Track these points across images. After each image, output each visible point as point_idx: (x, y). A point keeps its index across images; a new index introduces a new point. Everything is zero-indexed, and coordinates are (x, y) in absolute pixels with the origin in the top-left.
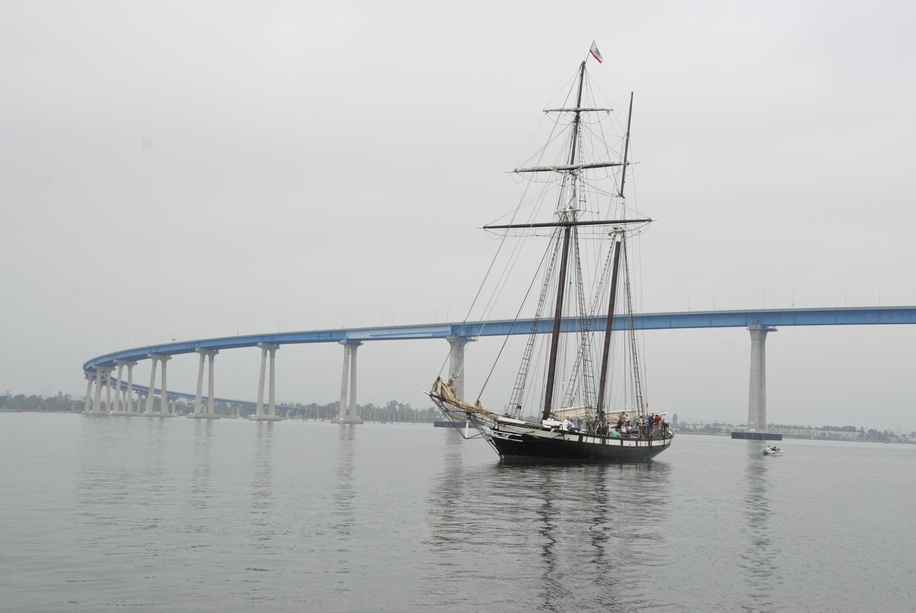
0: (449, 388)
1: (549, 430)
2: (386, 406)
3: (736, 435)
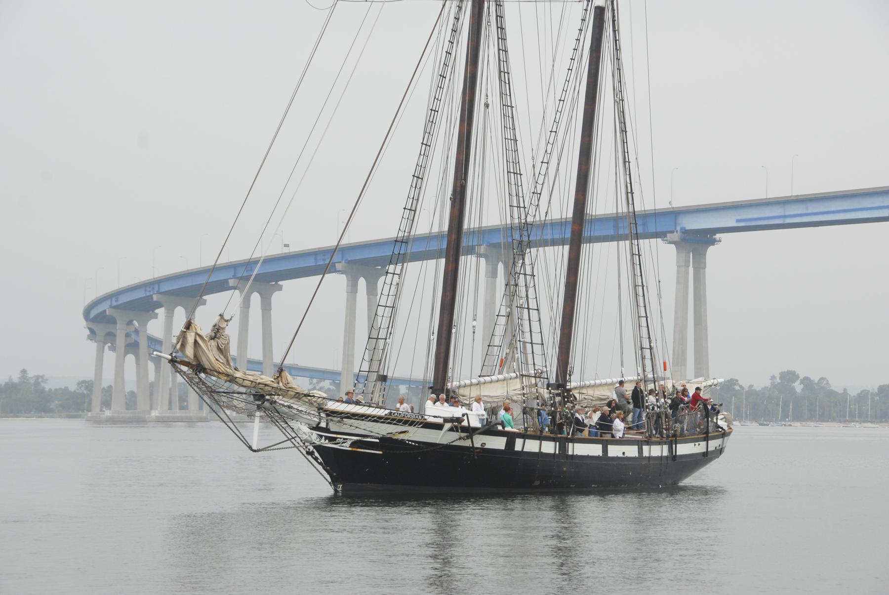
0: (213, 343)
1: (438, 427)
2: (767, 383)
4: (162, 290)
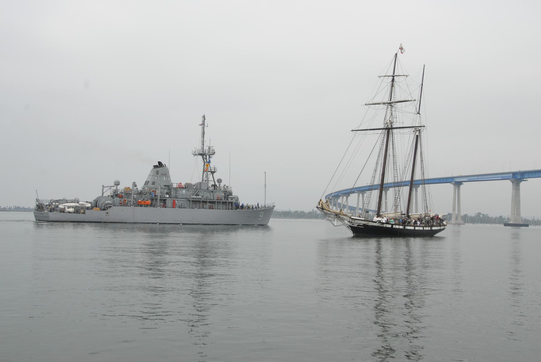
1: (376, 222)
2: (474, 215)
3: (506, 225)
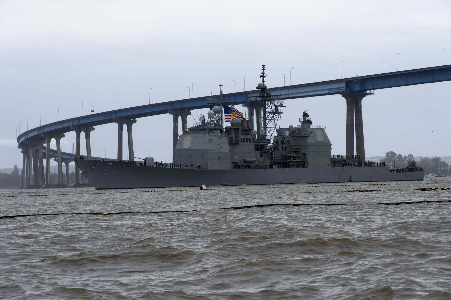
4: (74, 124)
